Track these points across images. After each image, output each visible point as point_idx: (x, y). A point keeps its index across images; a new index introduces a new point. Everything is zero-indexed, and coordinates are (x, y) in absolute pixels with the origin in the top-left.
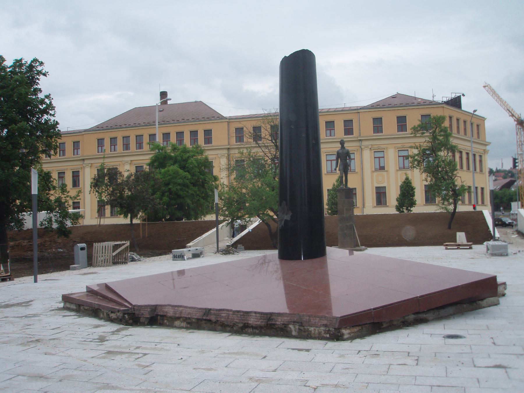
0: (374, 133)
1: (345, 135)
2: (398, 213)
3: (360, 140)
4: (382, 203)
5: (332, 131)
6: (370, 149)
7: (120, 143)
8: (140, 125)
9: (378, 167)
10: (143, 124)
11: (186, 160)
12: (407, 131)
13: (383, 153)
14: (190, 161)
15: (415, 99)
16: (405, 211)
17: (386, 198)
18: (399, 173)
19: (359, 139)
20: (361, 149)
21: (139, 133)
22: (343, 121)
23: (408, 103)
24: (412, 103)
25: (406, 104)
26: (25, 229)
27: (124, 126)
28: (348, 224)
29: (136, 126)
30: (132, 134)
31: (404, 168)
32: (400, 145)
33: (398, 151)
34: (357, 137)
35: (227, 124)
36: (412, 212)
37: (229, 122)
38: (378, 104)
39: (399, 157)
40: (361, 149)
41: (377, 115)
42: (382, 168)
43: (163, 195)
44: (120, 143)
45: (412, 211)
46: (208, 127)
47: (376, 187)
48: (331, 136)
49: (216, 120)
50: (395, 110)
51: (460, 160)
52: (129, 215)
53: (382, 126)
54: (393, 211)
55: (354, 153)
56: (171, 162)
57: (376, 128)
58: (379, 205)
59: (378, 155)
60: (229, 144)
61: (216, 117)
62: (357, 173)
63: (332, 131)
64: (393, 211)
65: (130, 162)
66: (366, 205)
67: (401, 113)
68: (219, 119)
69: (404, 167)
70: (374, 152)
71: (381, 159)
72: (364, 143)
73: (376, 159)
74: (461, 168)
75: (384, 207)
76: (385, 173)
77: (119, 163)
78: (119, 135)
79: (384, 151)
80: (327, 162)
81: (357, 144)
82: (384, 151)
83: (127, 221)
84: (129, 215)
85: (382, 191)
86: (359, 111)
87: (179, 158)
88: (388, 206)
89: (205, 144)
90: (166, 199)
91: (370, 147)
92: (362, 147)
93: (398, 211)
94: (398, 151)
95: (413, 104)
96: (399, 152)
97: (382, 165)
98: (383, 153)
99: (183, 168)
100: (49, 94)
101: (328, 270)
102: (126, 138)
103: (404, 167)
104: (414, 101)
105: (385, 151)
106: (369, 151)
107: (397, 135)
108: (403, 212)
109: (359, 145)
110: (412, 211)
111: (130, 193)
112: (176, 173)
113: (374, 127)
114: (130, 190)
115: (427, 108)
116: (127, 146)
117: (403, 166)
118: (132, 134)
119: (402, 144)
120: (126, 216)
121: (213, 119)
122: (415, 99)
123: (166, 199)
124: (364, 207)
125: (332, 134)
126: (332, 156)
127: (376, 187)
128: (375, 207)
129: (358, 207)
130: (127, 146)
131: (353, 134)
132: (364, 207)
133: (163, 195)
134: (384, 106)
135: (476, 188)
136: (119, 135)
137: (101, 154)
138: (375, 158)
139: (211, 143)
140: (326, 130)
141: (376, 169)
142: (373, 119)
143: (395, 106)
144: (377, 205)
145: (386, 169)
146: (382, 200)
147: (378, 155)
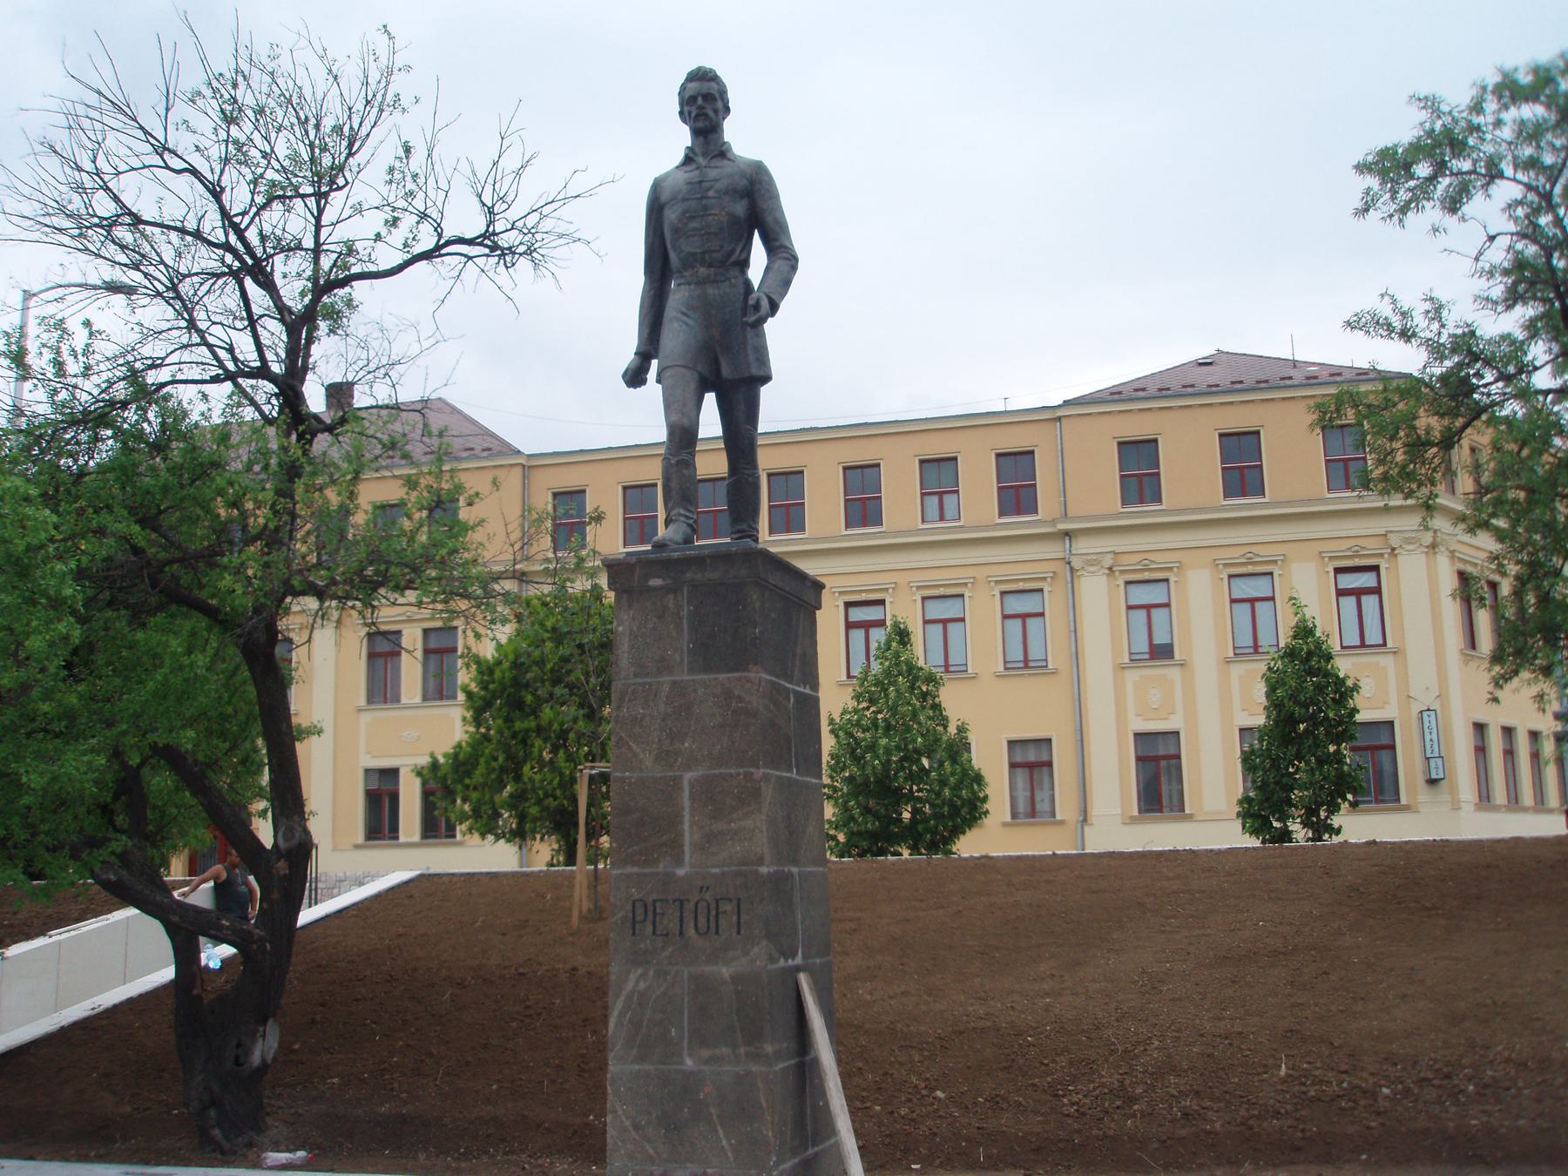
0: (1123, 504)
1: (1226, 496)
2: (1253, 842)
3: (1067, 534)
4: (1165, 802)
5: (949, 500)
6: (1110, 569)
9: (1146, 648)
12: (1036, 512)
13: (1163, 586)
15: (1295, 366)
16: (1299, 833)
17: (1180, 781)
18: (1237, 670)
19: (1062, 526)
20: (1072, 569)
22: (993, 457)
23: (1263, 378)
24: (1282, 379)
25: (1184, 387)
31: (1026, 667)
32: (1236, 553)
33: (1230, 576)
34: (1054, 522)
36: (1336, 839)
37: (529, 467)
38: (1137, 385)
39: (1235, 606)
40: (1072, 569)
41: (1136, 428)
42: (1161, 652)
45: (1338, 831)
47: (1137, 735)
48: (942, 518)
49: (478, 458)
50: (1211, 405)
51: (1466, 611)
53: (1158, 474)
54: (1233, 836)
55: (1041, 590)
57: (636, 524)
58: (1152, 811)
59: (1143, 595)
61: (479, 449)
62: (1054, 673)
63: (948, 499)
64: (1233, 836)
66: (1096, 811)
67: (1238, 420)
69: (1026, 660)
70: (1128, 583)
71: (1155, 612)
72: (1083, 546)
73: (1133, 613)
74: (1468, 642)
75: (1175, 819)
76: (1174, 674)
79: (1167, 580)
80: (928, 626)
81: (1053, 550)
82: (1167, 580)
85: (1161, 752)
86: (1059, 413)
88: (1190, 818)
89: (847, 527)
91: (1108, 561)
92: (1076, 563)
93: (1255, 832)
94: (1230, 576)
95: (1288, 382)
96: (1232, 581)
97: (1160, 638)
98: (1162, 587)
100: (1489, 196)
101: (66, 1159)
103: (1026, 660)
104: (1292, 373)
105: (1172, 579)
106: (1104, 578)
107: (1223, 508)
108: (1285, 835)
109: (1060, 555)
110: (1338, 831)
113: (1122, 477)
115: (478, 468)
117: (1022, 659)
119: (1247, 549)
122: (1295, 366)
124: (1085, 819)
125: (949, 513)
126: (950, 602)
127: (1137, 735)
128: (1133, 820)
129: (1062, 822)
132: (1085, 820)
134: (1164, 392)
135: (1508, 732)
137: (938, 531)
138: (1130, 608)
139: (802, 529)
140: (923, 495)
141: (1134, 657)
142: (1120, 444)
143: (1213, 390)
144: (1140, 812)
145: (1177, 656)
147: (1143, 595)
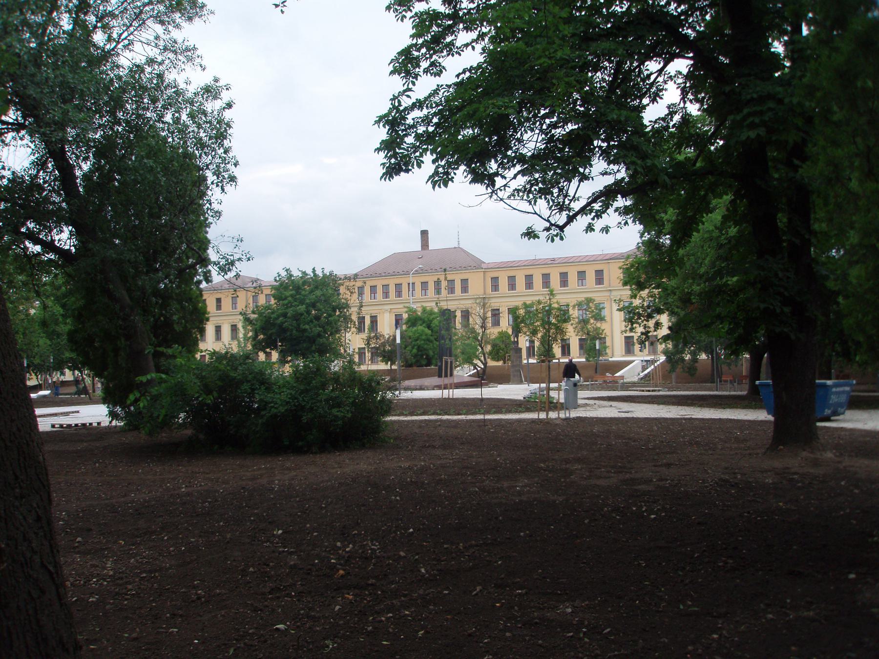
7: (380, 290)
8: (398, 274)
10: (402, 273)
11: (431, 321)
14: (433, 322)
21: (398, 281)
26: (669, 332)
27: (384, 274)
28: (432, 367)
29: (394, 274)
30: (392, 283)
35: (483, 273)
43: (413, 348)
44: (380, 290)
46: (464, 277)
48: (582, 285)
52: (389, 363)
56: (420, 322)
60: (485, 294)
65: (389, 310)
68: (476, 269)
77: (379, 311)
78: (379, 283)
81: (607, 294)
83: (388, 367)
84: (389, 363)
87: (426, 319)
90: (415, 351)
99: (429, 327)
102: (385, 287)
111: (390, 348)
112: (423, 331)
114: (389, 346)
116: (386, 294)
118: (392, 283)
120: (387, 364)
121: (469, 268)
123: (415, 351)
125: (584, 284)
130: (386, 294)
131: (603, 284)
133: (413, 348)
136: (379, 283)
146: (632, 348)
